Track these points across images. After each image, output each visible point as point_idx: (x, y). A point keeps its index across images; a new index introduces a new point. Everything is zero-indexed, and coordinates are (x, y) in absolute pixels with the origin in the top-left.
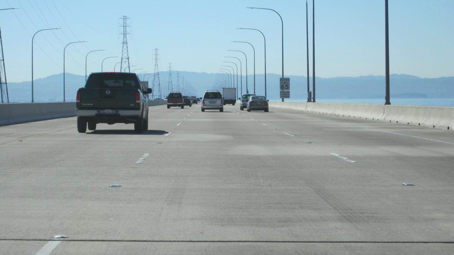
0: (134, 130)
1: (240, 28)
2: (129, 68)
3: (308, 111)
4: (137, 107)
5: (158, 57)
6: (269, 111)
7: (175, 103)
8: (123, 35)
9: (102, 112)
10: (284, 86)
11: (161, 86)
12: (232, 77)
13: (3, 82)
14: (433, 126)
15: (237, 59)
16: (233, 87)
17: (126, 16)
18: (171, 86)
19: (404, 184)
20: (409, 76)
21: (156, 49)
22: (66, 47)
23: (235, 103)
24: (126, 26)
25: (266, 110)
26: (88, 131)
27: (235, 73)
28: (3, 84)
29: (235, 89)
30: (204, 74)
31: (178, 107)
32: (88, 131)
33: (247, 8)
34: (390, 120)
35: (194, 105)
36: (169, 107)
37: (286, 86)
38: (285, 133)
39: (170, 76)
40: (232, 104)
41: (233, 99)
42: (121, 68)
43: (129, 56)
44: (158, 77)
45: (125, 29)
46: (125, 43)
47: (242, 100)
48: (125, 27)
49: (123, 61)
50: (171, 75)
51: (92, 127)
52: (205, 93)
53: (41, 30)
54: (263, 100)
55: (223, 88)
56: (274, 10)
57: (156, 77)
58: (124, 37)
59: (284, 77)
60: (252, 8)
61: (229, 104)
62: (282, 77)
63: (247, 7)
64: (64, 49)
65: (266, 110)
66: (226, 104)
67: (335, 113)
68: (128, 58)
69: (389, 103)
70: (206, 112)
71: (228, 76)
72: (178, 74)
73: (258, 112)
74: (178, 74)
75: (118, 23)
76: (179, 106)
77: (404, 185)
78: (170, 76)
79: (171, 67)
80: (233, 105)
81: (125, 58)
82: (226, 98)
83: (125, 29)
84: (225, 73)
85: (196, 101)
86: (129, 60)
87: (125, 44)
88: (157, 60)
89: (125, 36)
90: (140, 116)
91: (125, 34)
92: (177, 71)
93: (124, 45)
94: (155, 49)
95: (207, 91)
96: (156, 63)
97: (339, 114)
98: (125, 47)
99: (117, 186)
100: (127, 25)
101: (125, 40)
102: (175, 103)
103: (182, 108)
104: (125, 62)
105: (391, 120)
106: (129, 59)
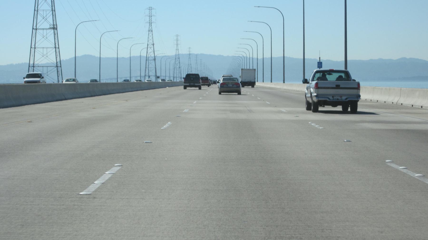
1: (258, 6)
5: (153, 19)
7: (204, 84)
9: (190, 84)
12: (248, 59)
13: (59, 66)
14: (412, 106)
16: (252, 68)
17: (151, 7)
18: (190, 68)
20: (418, 59)
21: (177, 35)
22: (78, 26)
23: (254, 85)
24: (151, 16)
27: (251, 56)
28: (59, 67)
29: (255, 70)
31: (206, 86)
33: (255, 7)
34: (421, 105)
35: (213, 86)
36: (185, 88)
39: (151, 34)
40: (251, 87)
41: (253, 81)
42: (147, 52)
43: (154, 43)
44: (179, 60)
45: (150, 18)
46: (150, 31)
47: (317, 84)
49: (148, 47)
50: (190, 58)
53: (104, 33)
54: (235, 82)
55: (242, 69)
56: (279, 9)
57: (177, 60)
58: (149, 25)
60: (259, 7)
61: (248, 86)
63: (255, 6)
64: (76, 28)
66: (245, 87)
68: (153, 44)
70: (222, 94)
73: (248, 88)
75: (145, 13)
76: (207, 85)
77: (345, 141)
78: (151, 34)
80: (252, 87)
81: (151, 44)
82: (245, 80)
83: (150, 18)
84: (241, 56)
85: (215, 82)
89: (150, 25)
91: (150, 23)
93: (149, 33)
94: (149, 8)
95: (224, 75)
96: (150, 28)
97: (372, 99)
100: (152, 15)
102: (204, 84)
103: (200, 88)
104: (150, 48)
105: (413, 104)
106: (154, 45)
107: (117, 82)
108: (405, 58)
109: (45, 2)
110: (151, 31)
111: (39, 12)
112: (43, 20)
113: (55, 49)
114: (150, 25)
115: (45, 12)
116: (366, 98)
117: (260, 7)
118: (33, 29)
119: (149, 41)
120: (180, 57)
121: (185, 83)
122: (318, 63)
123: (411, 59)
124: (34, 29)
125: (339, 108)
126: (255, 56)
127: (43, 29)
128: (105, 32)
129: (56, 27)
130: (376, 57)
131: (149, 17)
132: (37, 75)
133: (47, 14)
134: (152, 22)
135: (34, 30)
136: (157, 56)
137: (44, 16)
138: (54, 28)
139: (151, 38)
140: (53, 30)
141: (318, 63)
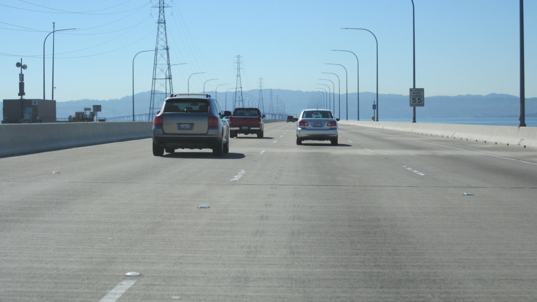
3: (508, 145)
4: (259, 125)
8: (237, 70)
10: (417, 99)
11: (264, 108)
15: (331, 82)
17: (239, 55)
21: (239, 56)
26: (165, 153)
30: (299, 93)
32: (165, 153)
36: (288, 122)
37: (418, 100)
38: (417, 172)
39: (261, 93)
48: (238, 63)
51: (236, 136)
54: (333, 119)
58: (160, 12)
59: (416, 87)
60: (347, 29)
62: (412, 87)
67: (454, 136)
69: (525, 125)
71: (323, 95)
72: (271, 92)
74: (271, 92)
78: (162, 30)
79: (261, 83)
83: (239, 65)
88: (240, 70)
89: (239, 71)
91: (239, 69)
92: (269, 89)
93: (160, 26)
98: (239, 79)
99: (205, 208)
101: (162, 17)
105: (486, 141)
107: (134, 120)
108: (495, 94)
111: (157, 65)
112: (161, 72)
114: (239, 71)
115: (162, 66)
116: (402, 130)
118: (153, 79)
119: (238, 85)
120: (242, 86)
121: (288, 119)
122: (373, 105)
123: (501, 95)
126: (337, 92)
127: (161, 79)
130: (464, 93)
132: (29, 110)
134: (240, 68)
136: (228, 91)
137: (162, 69)
139: (239, 82)
140: (169, 80)
141: (373, 105)
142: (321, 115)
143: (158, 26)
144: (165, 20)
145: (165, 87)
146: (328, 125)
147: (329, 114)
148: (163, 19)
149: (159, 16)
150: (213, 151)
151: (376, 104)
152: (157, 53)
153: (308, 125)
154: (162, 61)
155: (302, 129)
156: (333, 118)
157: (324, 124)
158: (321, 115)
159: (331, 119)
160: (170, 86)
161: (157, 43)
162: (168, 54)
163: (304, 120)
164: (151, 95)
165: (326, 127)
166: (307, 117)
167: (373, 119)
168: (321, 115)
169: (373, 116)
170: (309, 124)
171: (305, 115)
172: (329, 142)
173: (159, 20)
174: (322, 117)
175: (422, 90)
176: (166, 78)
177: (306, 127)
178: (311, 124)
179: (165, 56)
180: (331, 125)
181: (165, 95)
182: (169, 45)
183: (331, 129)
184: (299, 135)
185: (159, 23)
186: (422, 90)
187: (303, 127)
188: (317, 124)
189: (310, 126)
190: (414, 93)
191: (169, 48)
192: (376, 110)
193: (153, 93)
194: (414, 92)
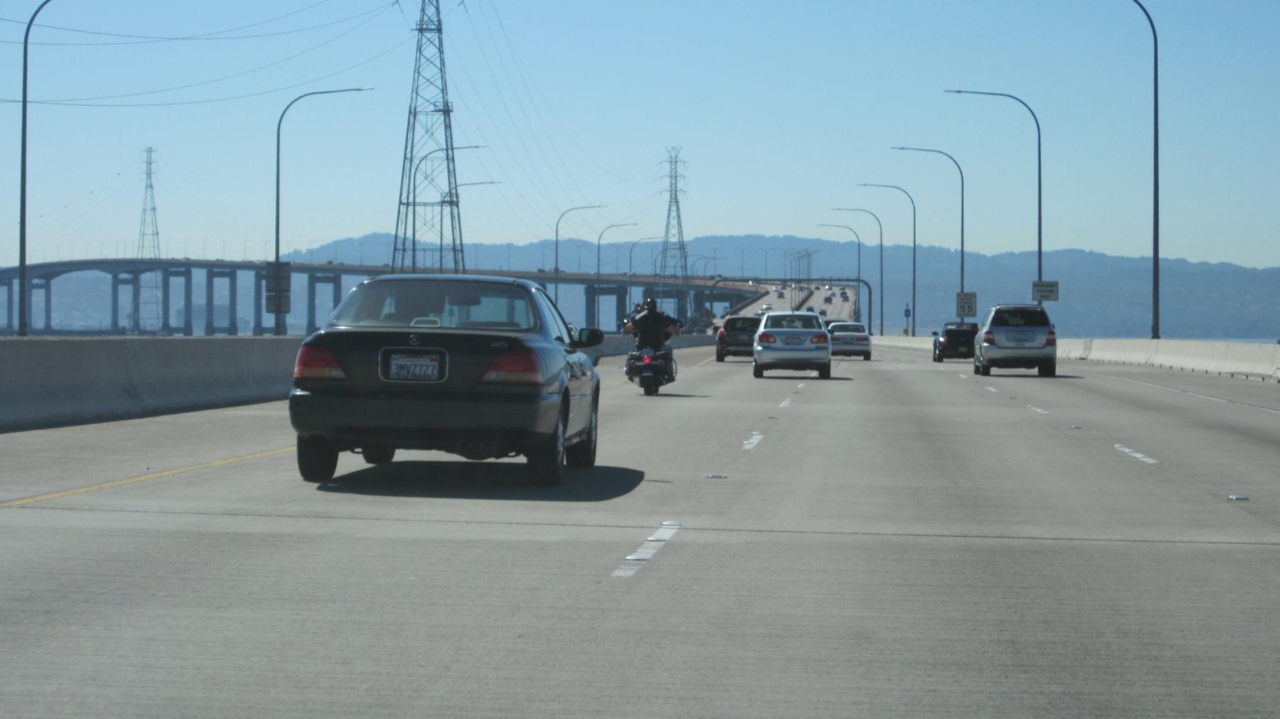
0: (524, 464)
2: (450, 159)
6: (1059, 371)
19: (1231, 497)
25: (867, 356)
33: (945, 91)
52: (993, 313)
59: (965, 291)
60: (959, 92)
62: (1036, 279)
65: (867, 356)
70: (727, 362)
77: (1232, 499)
78: (430, 51)
86: (554, 262)
87: (428, 35)
90: (643, 288)
93: (424, 40)
97: (1209, 370)
109: (430, 139)
110: (433, 27)
112: (426, 182)
113: (452, 253)
117: (964, 92)
118: (401, 203)
124: (404, 204)
125: (1035, 371)
128: (430, 151)
129: (455, 199)
131: (669, 163)
133: (434, 168)
135: (402, 206)
138: (451, 203)
140: (449, 207)
142: (801, 323)
143: (419, 41)
144: (439, 21)
145: (439, 229)
146: (812, 342)
147: (815, 322)
148: (436, 19)
149: (423, 10)
150: (528, 460)
151: (911, 308)
152: (414, 125)
153: (775, 341)
154: (429, 143)
155: (765, 348)
156: (821, 328)
157: (805, 341)
158: (801, 323)
159: (820, 330)
160: (453, 229)
161: (415, 90)
162: (448, 127)
163: (768, 331)
164: (394, 253)
165: (808, 344)
166: (773, 326)
167: (906, 332)
168: (798, 324)
169: (905, 328)
170: (778, 339)
171: (770, 321)
172: (815, 373)
173: (422, 20)
174: (804, 327)
175: (974, 295)
176: (443, 203)
177: (772, 345)
178: (781, 340)
179: (440, 134)
180: (817, 342)
181: (438, 253)
182: (451, 98)
183: (818, 349)
184: (758, 361)
185: (421, 30)
186: (974, 295)
187: (767, 344)
188: (792, 340)
189: (779, 344)
190: (963, 299)
191: (450, 108)
192: (910, 319)
193: (400, 247)
194: (963, 297)
